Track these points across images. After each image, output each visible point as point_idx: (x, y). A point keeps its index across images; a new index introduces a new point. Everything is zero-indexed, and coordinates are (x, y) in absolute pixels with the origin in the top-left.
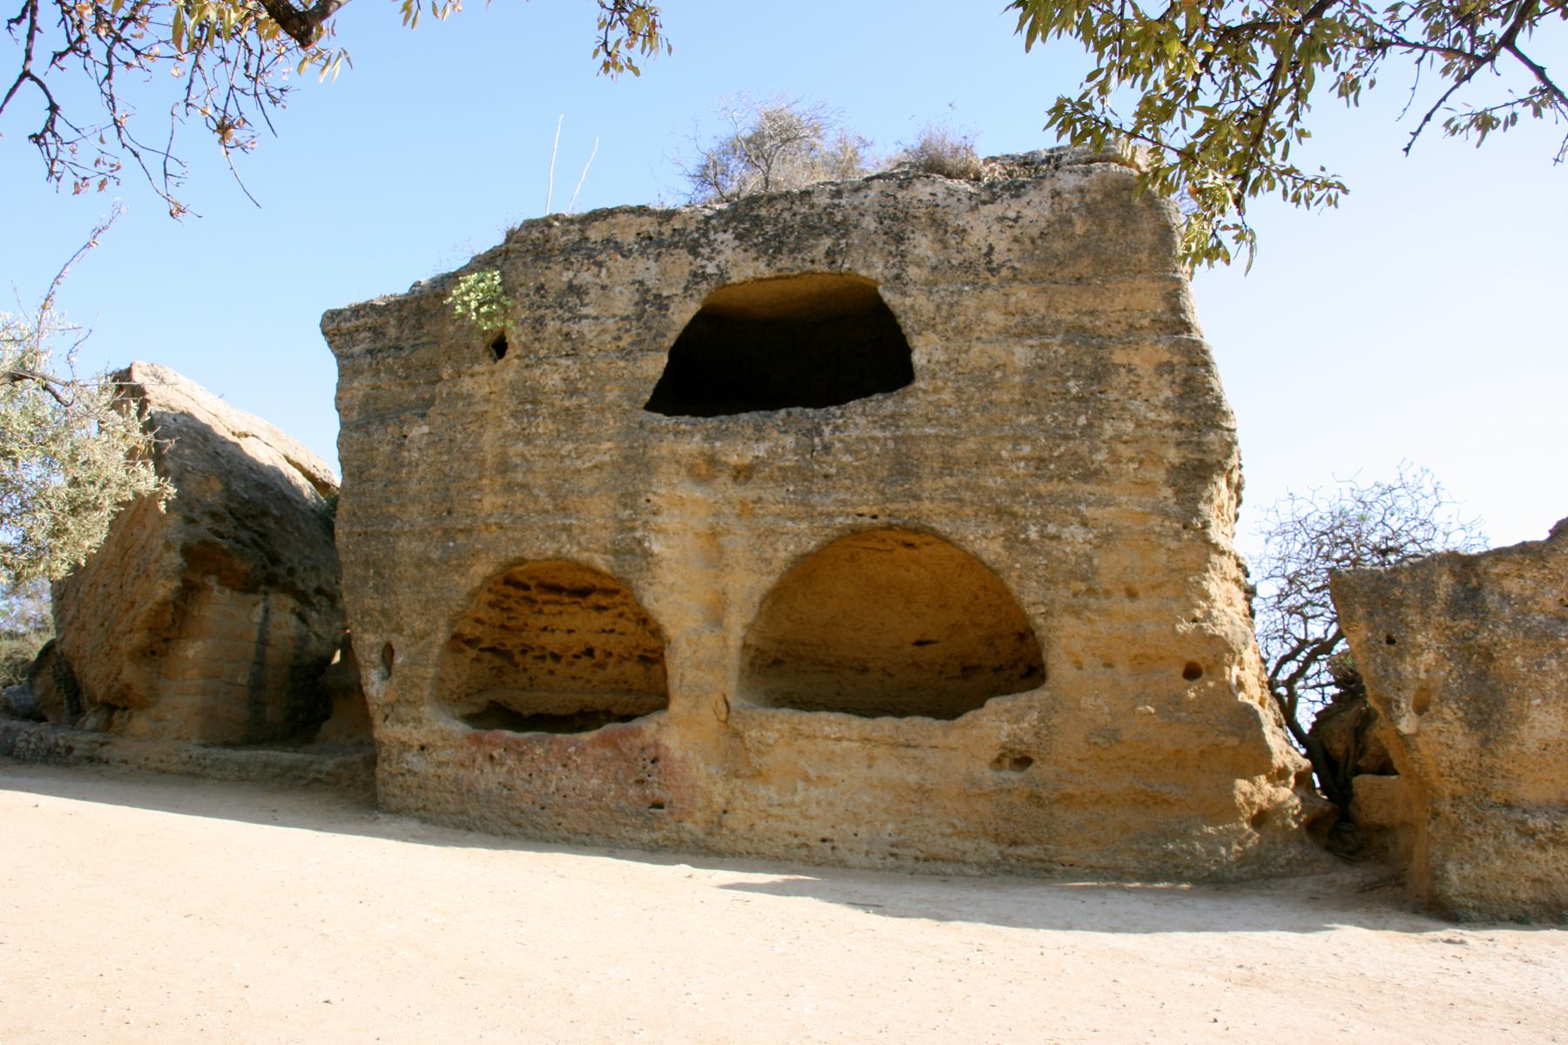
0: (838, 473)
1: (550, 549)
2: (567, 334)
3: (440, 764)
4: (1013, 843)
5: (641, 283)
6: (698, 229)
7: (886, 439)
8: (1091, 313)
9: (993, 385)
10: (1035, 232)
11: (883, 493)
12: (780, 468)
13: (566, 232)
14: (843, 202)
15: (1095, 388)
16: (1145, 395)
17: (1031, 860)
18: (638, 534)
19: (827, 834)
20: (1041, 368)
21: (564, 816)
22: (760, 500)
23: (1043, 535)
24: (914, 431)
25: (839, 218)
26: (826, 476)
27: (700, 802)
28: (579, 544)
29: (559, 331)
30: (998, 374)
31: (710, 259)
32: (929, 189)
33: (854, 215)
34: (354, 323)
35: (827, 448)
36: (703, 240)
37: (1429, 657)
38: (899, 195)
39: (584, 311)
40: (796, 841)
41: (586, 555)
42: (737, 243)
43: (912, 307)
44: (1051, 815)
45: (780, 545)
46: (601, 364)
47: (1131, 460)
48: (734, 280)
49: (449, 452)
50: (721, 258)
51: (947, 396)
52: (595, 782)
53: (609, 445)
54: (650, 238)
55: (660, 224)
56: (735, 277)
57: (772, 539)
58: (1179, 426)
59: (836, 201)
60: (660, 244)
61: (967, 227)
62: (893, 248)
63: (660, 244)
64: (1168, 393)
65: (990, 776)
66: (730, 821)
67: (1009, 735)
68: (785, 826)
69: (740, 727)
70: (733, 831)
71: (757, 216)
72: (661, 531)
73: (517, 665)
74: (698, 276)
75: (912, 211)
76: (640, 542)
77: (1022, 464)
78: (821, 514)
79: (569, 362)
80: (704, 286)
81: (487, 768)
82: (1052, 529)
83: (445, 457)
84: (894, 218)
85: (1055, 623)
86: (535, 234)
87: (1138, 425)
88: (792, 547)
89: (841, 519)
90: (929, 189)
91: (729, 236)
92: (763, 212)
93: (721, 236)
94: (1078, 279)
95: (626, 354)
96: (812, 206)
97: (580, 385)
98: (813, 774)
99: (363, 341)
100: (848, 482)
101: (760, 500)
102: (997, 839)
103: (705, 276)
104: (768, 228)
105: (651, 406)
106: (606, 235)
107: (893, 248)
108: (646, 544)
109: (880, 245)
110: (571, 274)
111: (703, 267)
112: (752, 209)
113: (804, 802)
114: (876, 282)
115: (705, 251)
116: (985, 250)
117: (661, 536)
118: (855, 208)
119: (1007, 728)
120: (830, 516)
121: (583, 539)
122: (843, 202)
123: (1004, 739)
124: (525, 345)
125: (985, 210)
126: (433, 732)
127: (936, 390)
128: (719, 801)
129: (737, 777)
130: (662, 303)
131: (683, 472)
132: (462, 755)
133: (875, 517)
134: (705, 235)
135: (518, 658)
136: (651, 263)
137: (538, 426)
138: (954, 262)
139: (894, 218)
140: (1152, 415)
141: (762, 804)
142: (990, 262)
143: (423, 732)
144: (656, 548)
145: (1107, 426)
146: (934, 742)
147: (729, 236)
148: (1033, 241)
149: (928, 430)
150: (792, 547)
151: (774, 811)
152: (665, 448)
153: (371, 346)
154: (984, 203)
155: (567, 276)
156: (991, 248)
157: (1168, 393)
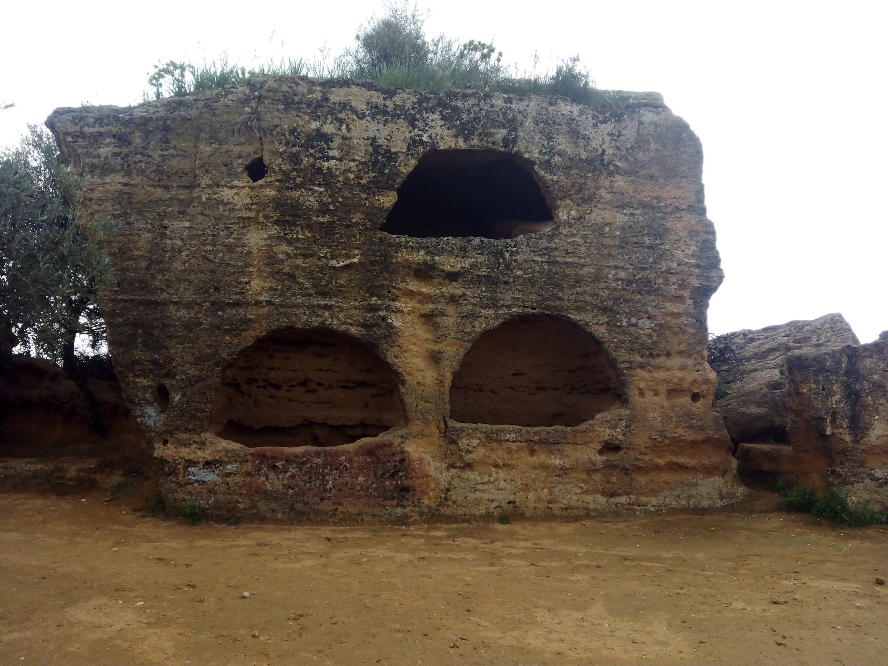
0: (514, 282)
1: (316, 321)
2: (319, 168)
3: (228, 475)
4: (612, 495)
5: (374, 140)
6: (414, 108)
7: (542, 262)
8: (657, 198)
9: (603, 235)
10: (629, 145)
11: (541, 296)
12: (478, 276)
13: (310, 91)
14: (513, 106)
15: (657, 242)
16: (683, 247)
17: (623, 504)
18: (383, 313)
19: (511, 498)
20: (630, 227)
21: (340, 504)
22: (464, 294)
23: (629, 324)
24: (559, 259)
25: (510, 117)
26: (506, 283)
27: (432, 485)
28: (339, 319)
29: (313, 166)
30: (607, 229)
31: (425, 131)
32: (569, 108)
33: (520, 117)
34: (97, 129)
35: (507, 266)
36: (418, 117)
37: (838, 397)
38: (550, 109)
39: (331, 153)
40: (494, 505)
41: (344, 326)
42: (442, 123)
43: (558, 181)
44: (632, 479)
45: (476, 324)
46: (347, 194)
47: (674, 283)
48: (442, 148)
49: (213, 244)
50: (431, 131)
51: (577, 239)
52: (361, 479)
53: (357, 251)
54: (377, 107)
55: (385, 99)
56: (442, 146)
57: (471, 320)
58: (698, 266)
59: (508, 105)
60: (385, 113)
61: (591, 136)
62: (545, 143)
63: (385, 113)
64: (693, 248)
65: (599, 459)
66: (453, 495)
67: (609, 435)
68: (486, 496)
69: (455, 437)
70: (455, 502)
71: (456, 106)
72: (399, 311)
73: (243, 392)
74: (415, 142)
75: (558, 121)
76: (384, 319)
77: (620, 283)
78: (503, 306)
79: (322, 190)
80: (421, 149)
81: (272, 475)
82: (634, 320)
83: (209, 248)
84: (546, 122)
85: (633, 373)
86: (285, 88)
87: (679, 265)
88: (484, 325)
89: (515, 310)
90: (569, 108)
91: (436, 116)
92: (459, 104)
93: (432, 117)
94: (651, 177)
95: (365, 188)
96: (492, 106)
97: (331, 207)
98: (500, 462)
99: (108, 145)
100: (520, 287)
101: (464, 294)
102: (603, 493)
103: (422, 142)
104: (464, 116)
105: (383, 228)
106: (343, 99)
107: (545, 143)
108: (389, 321)
109: (537, 139)
110: (318, 124)
111: (419, 136)
112: (451, 101)
113: (496, 480)
114: (534, 163)
115: (420, 124)
116: (600, 152)
117: (398, 315)
118: (520, 112)
119: (608, 431)
120: (509, 307)
121: (341, 316)
122: (513, 106)
123: (607, 438)
124: (283, 172)
125: (602, 127)
126: (218, 451)
127: (572, 235)
128: (444, 484)
129: (454, 467)
130: (391, 156)
131: (412, 274)
132: (248, 467)
133: (534, 309)
134: (420, 113)
135: (244, 387)
136: (381, 126)
137: (297, 233)
138: (582, 157)
139: (546, 122)
140: (686, 260)
141: (472, 484)
142: (603, 160)
143: (208, 451)
144: (396, 324)
145: (664, 264)
146: (568, 440)
147: (436, 116)
148: (627, 150)
149: (568, 260)
150: (484, 325)
151: (480, 487)
152: (403, 255)
153: (117, 150)
154: (602, 123)
155: (314, 125)
156: (604, 151)
157: (693, 248)
